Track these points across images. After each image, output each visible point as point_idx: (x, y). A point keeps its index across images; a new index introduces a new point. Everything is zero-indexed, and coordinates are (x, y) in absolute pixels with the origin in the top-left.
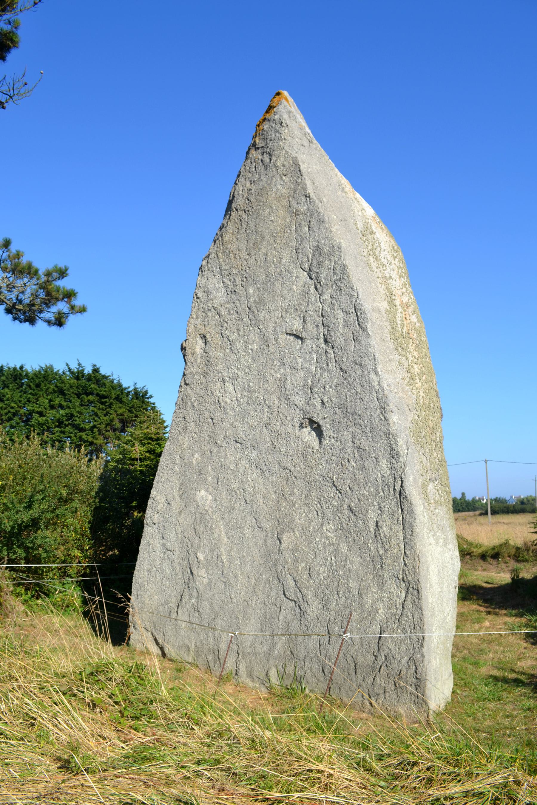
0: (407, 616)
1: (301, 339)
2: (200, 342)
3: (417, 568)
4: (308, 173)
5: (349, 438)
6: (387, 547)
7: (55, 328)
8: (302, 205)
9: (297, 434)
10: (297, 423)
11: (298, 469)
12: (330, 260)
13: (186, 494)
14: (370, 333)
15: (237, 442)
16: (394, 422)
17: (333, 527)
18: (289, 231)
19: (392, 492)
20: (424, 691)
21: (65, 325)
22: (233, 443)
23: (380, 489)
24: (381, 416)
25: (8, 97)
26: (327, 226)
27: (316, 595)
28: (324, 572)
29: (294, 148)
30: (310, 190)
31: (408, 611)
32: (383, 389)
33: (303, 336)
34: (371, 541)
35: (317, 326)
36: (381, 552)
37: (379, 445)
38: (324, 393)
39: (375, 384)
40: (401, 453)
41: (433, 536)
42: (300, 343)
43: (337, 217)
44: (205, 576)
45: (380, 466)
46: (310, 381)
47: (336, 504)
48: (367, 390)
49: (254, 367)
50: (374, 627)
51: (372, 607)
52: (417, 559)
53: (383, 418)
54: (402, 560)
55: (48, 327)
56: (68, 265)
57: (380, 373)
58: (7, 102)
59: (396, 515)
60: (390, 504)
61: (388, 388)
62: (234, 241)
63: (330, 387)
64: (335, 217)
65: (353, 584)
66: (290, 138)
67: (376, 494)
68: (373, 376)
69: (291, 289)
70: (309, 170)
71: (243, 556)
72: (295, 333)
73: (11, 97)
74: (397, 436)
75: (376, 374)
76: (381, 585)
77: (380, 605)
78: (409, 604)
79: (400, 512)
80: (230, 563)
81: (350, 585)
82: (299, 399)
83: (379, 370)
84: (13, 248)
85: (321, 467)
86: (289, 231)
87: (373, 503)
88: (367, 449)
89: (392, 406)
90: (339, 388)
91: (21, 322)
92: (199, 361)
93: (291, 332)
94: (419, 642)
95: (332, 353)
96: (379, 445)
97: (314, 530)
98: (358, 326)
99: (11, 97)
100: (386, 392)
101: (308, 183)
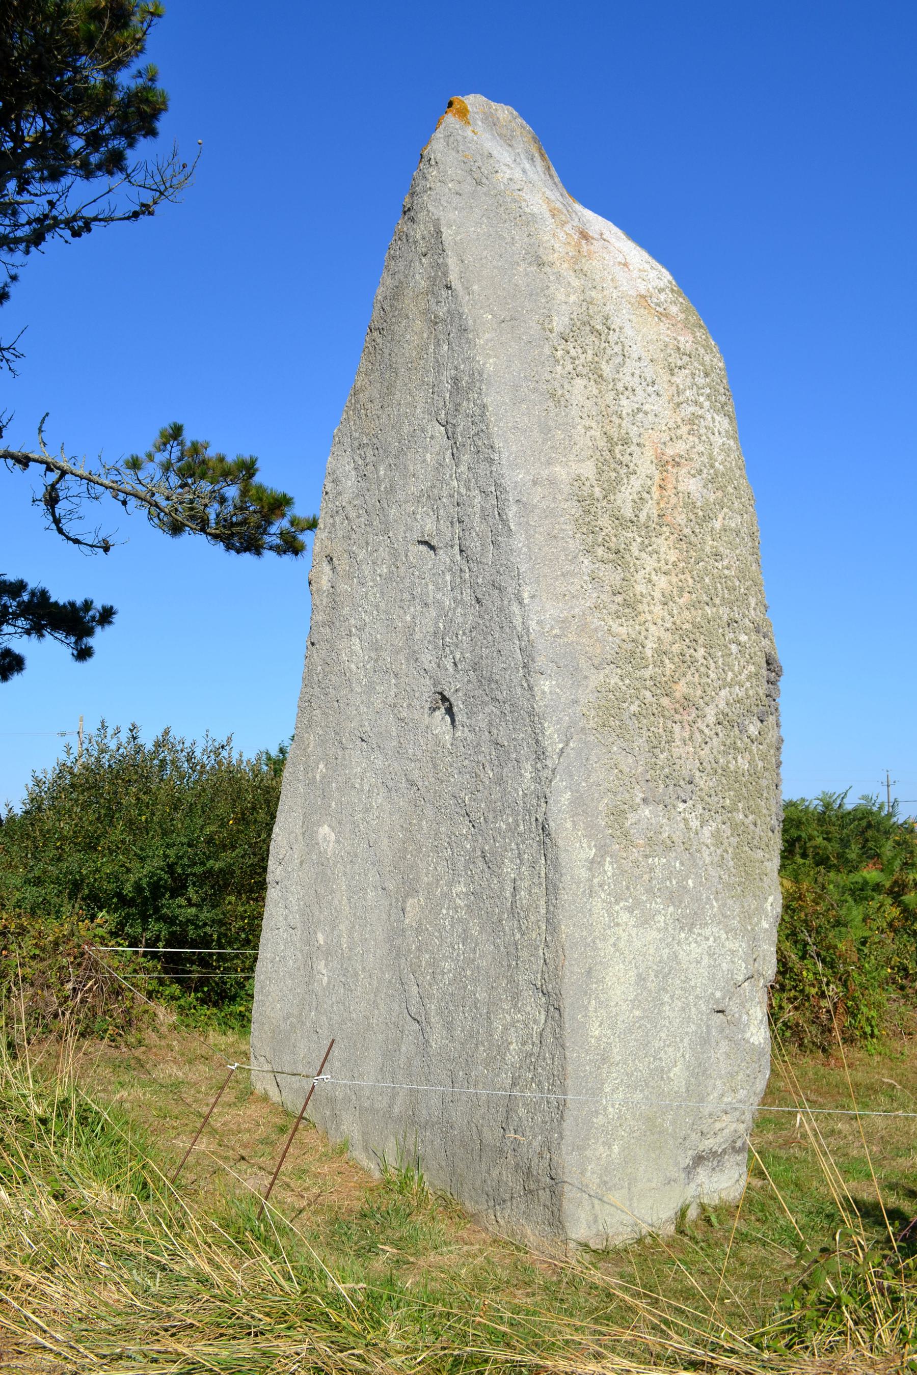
0: (545, 1059)
1: (432, 548)
2: (327, 568)
3: (560, 968)
4: (455, 243)
5: (483, 725)
6: (523, 928)
7: (288, 558)
8: (443, 304)
9: (426, 723)
10: (427, 701)
11: (426, 783)
12: (468, 400)
13: (309, 833)
14: (512, 527)
15: (363, 740)
16: (544, 692)
17: (464, 890)
18: (425, 356)
19: (534, 823)
20: (561, 1206)
21: (304, 552)
22: (358, 742)
23: (520, 817)
24: (524, 682)
25: (158, 194)
26: (470, 336)
27: (440, 1012)
28: (450, 971)
29: (442, 202)
30: (453, 277)
31: (547, 1050)
32: (528, 631)
33: (436, 544)
34: (506, 916)
35: (452, 523)
36: (518, 936)
37: (521, 735)
38: (456, 645)
39: (518, 621)
40: (549, 749)
41: (630, 910)
42: (433, 556)
43: (494, 316)
44: (324, 972)
45: (521, 775)
46: (441, 625)
47: (468, 846)
48: (507, 633)
49: (382, 605)
50: (504, 1076)
51: (502, 1038)
52: (560, 952)
53: (525, 685)
54: (541, 951)
55: (278, 557)
56: (255, 455)
57: (526, 601)
58: (155, 203)
59: (538, 868)
60: (531, 848)
61: (537, 628)
62: (367, 386)
63: (464, 634)
64: (490, 317)
65: (481, 995)
66: (439, 184)
67: (515, 829)
68: (515, 608)
69: (424, 461)
70: (459, 238)
71: (366, 939)
72: (427, 539)
73: (162, 193)
74: (544, 718)
75: (521, 603)
76: (516, 997)
77: (512, 1036)
78: (548, 1034)
79: (543, 862)
80: (350, 950)
81: (477, 995)
82: (427, 659)
83: (526, 595)
84: (188, 437)
85: (452, 780)
86: (425, 356)
87: (510, 844)
88: (506, 744)
89: (541, 661)
90: (474, 634)
91: (238, 552)
92: (324, 603)
93: (423, 540)
94: (558, 1108)
95: (467, 570)
96: (521, 735)
97: (442, 892)
98: (497, 516)
99: (162, 193)
100: (532, 637)
101: (452, 262)
